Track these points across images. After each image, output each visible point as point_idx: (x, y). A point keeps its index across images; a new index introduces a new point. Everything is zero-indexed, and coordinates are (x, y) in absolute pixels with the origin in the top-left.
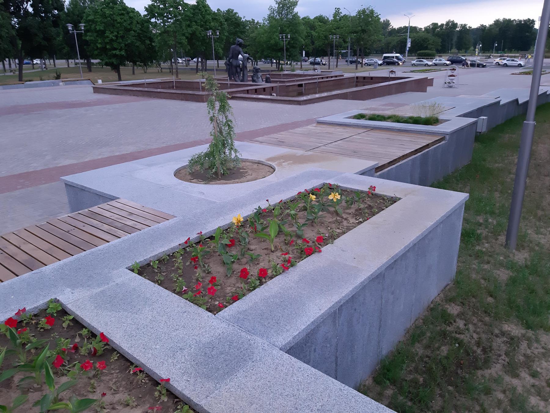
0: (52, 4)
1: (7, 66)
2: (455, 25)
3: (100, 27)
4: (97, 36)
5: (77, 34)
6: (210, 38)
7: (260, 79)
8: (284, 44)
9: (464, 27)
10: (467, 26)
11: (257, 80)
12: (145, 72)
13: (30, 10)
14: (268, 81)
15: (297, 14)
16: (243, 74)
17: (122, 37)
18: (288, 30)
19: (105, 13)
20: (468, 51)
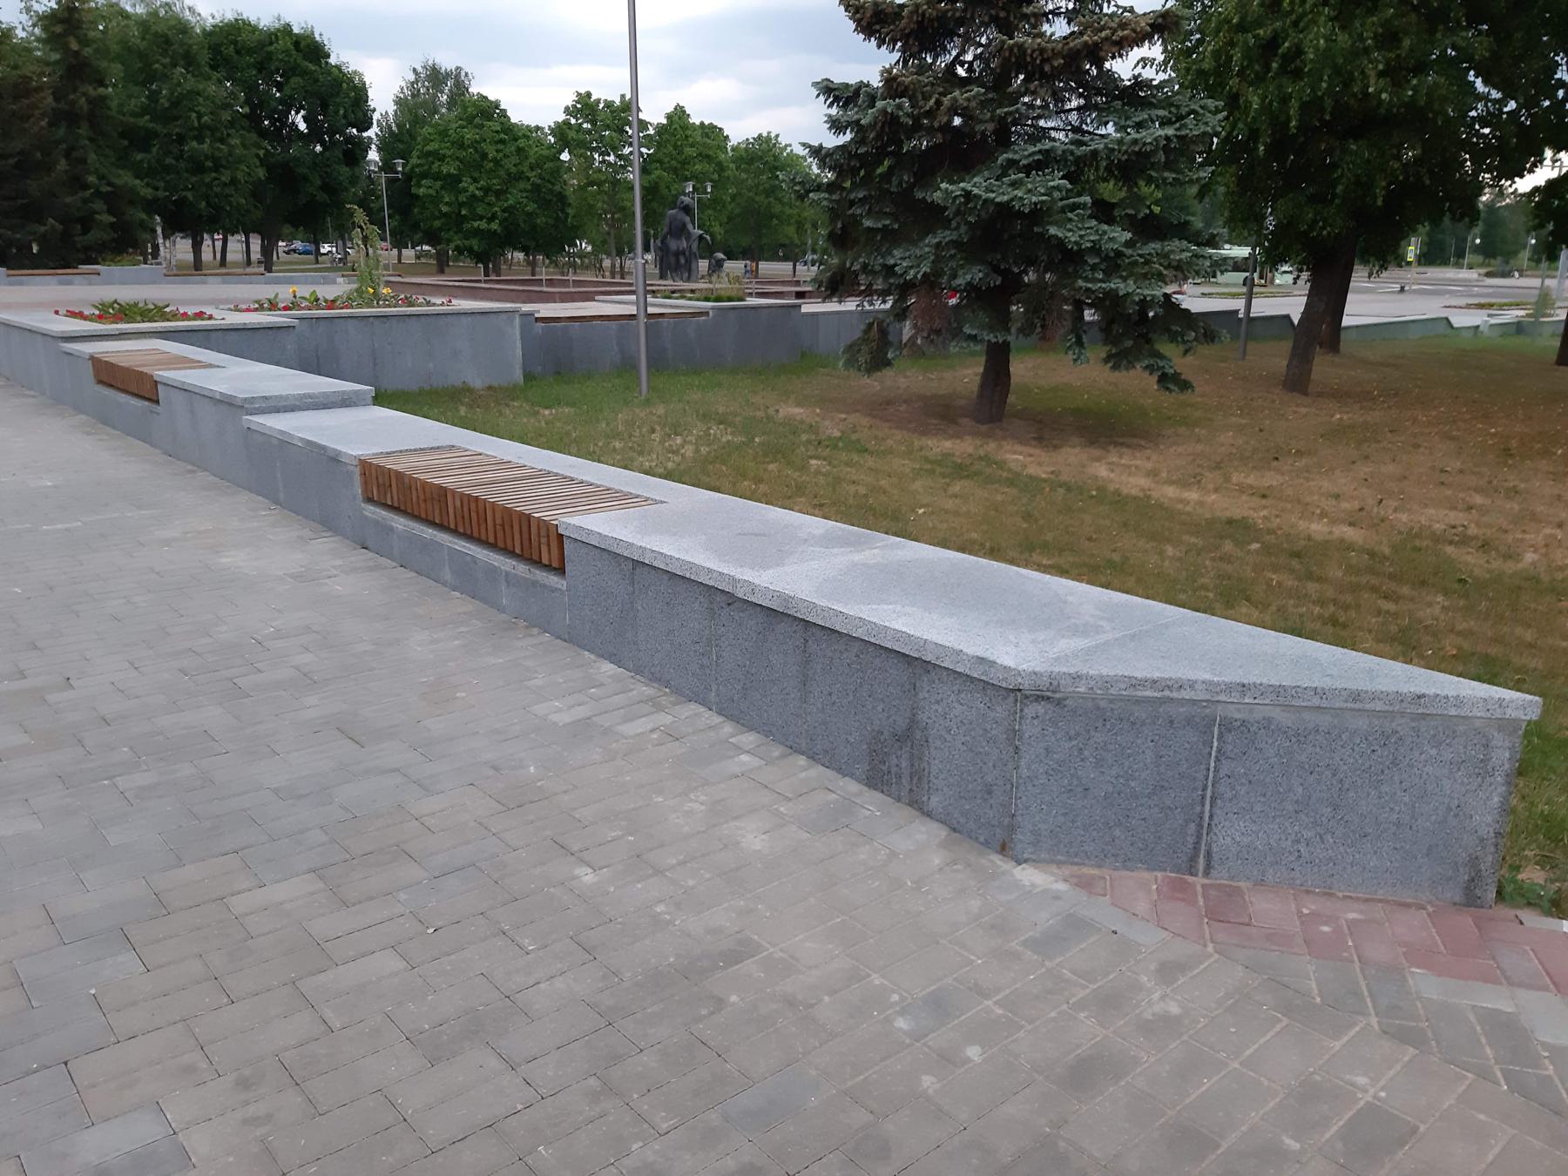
0: (345, 117)
1: (207, 254)
3: (449, 168)
4: (442, 188)
5: (388, 181)
10: (832, 141)
13: (302, 126)
17: (498, 194)
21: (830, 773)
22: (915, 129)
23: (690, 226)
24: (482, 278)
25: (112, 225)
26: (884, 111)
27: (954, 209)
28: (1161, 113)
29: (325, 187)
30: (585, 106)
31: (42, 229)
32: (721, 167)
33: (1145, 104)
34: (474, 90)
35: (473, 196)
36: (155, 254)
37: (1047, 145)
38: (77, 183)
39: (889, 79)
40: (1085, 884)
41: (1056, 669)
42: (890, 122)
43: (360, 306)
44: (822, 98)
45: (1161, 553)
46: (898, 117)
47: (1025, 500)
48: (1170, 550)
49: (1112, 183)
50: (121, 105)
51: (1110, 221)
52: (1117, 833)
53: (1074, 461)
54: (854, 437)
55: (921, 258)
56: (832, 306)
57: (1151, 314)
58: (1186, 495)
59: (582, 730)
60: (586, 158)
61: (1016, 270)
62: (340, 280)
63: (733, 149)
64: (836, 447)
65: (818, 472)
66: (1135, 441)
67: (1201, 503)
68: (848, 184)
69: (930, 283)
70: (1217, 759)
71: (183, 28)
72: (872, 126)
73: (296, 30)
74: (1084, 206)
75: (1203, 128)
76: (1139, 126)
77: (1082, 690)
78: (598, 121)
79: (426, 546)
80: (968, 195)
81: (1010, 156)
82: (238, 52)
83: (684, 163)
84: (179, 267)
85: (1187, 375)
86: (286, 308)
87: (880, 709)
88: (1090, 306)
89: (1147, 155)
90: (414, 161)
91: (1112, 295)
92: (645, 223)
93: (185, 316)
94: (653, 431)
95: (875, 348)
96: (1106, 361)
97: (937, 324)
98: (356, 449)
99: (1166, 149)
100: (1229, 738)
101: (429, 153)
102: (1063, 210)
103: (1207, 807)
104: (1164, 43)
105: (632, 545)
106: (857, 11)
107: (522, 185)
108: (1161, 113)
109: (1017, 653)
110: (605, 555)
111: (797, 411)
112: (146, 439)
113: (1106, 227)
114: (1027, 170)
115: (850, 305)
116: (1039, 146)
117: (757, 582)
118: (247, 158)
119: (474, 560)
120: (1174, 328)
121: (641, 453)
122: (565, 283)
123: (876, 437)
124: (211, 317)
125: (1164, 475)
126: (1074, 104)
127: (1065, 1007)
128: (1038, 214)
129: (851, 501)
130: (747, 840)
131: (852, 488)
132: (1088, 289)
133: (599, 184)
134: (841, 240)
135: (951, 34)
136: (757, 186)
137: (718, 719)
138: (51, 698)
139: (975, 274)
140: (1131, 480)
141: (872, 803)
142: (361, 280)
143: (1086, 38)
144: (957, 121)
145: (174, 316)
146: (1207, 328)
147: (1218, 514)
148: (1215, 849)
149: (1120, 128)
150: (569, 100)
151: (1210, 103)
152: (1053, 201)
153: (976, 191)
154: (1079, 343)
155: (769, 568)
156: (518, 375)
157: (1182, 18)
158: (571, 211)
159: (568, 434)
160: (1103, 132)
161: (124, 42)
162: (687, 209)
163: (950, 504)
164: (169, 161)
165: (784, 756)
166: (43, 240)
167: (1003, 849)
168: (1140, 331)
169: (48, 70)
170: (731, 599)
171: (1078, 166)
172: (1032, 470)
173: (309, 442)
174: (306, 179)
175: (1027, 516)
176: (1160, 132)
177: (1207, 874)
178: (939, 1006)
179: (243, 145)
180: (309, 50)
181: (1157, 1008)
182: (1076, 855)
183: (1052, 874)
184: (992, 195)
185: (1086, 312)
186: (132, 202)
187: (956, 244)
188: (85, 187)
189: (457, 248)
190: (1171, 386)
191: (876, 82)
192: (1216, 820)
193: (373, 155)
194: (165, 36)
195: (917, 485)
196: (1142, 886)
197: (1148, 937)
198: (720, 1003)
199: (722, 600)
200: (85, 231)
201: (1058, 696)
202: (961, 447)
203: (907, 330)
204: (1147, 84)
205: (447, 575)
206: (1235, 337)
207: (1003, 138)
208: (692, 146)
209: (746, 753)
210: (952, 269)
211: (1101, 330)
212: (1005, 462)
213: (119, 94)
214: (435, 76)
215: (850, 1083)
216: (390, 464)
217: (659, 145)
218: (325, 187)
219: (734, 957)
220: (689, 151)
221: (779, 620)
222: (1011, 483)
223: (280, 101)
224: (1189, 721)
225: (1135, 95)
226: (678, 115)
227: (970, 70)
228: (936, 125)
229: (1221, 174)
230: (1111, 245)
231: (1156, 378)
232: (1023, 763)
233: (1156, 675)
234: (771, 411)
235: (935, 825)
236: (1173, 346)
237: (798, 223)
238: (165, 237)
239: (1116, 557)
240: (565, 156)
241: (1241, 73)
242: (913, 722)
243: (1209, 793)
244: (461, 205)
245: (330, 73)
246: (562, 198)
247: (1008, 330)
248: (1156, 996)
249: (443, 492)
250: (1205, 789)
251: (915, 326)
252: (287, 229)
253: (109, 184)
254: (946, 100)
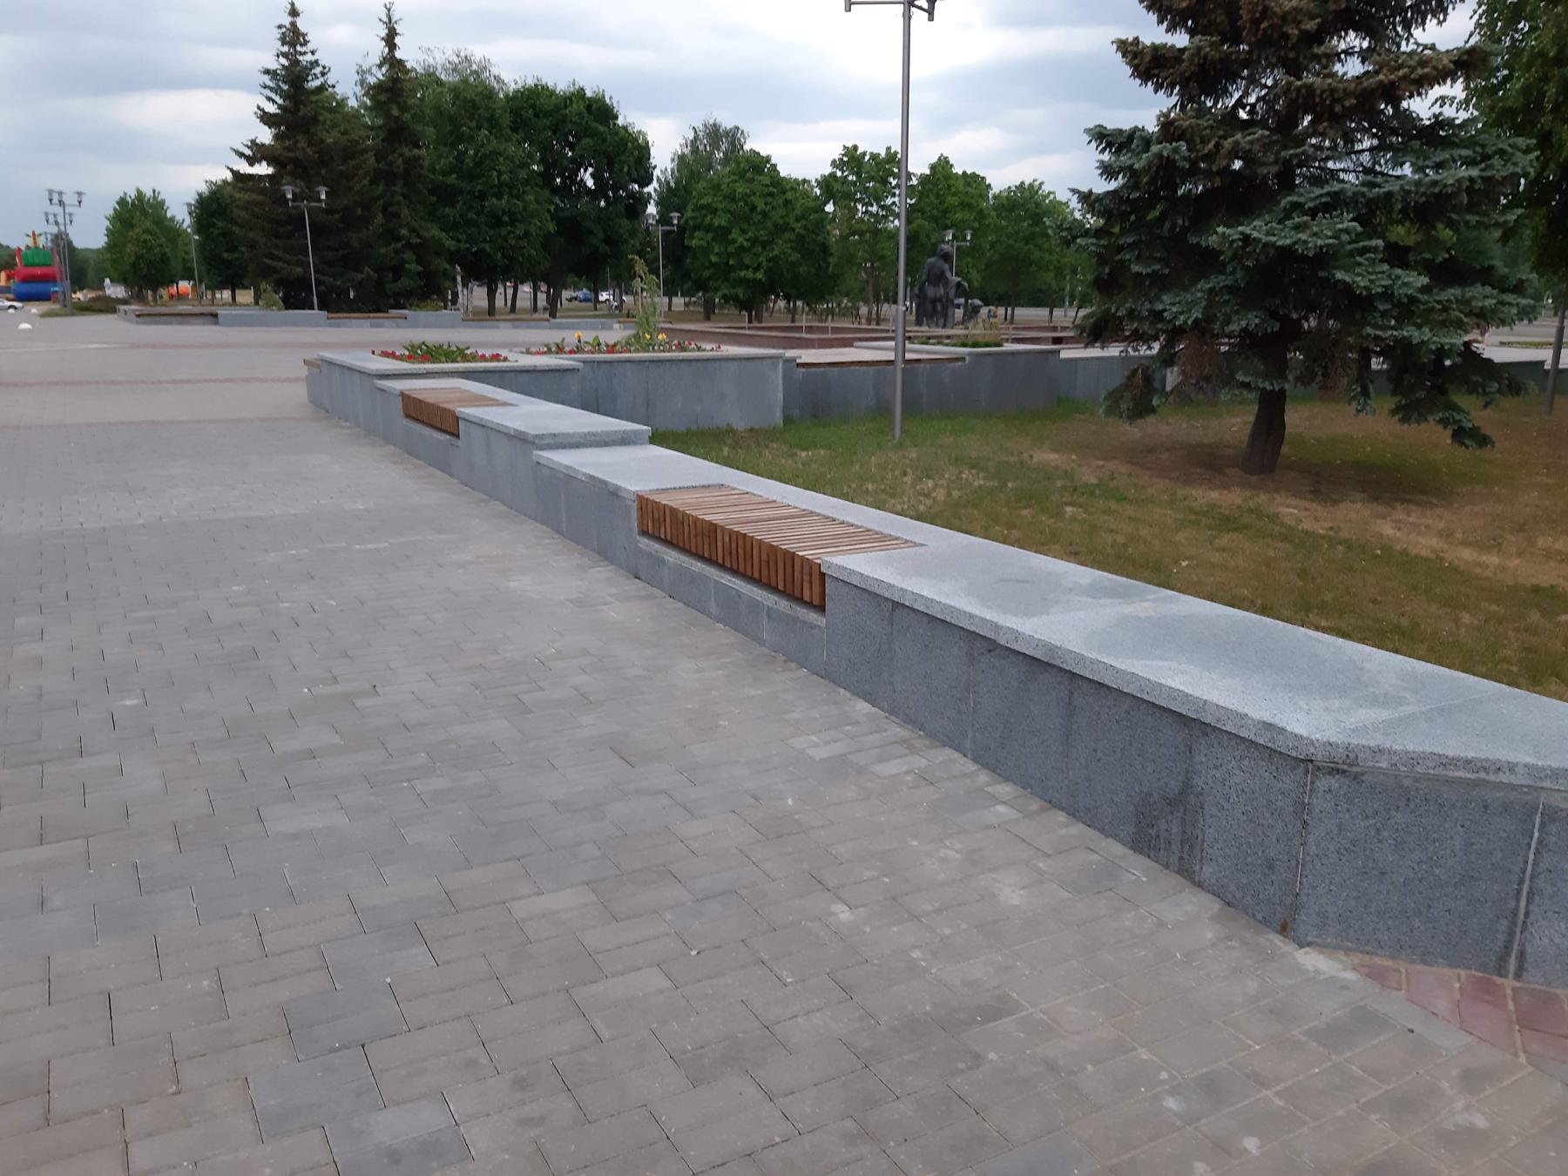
0: (629, 173)
1: (499, 302)
3: (721, 221)
10: (1102, 186)
13: (590, 183)
17: (764, 245)
21: (1091, 832)
22: (1192, 173)
23: (948, 274)
24: (746, 324)
25: (419, 273)
26: (1159, 156)
27: (1230, 254)
28: (1465, 152)
29: (608, 240)
30: (852, 159)
31: (359, 277)
32: (981, 215)
33: (1446, 143)
34: (747, 147)
35: (742, 247)
36: (455, 301)
37: (1336, 187)
38: (391, 235)
39: (1168, 127)
40: (1377, 975)
41: (1355, 741)
42: (1166, 171)
43: (637, 351)
44: (1094, 144)
45: (1457, 621)
46: (1174, 161)
47: (1299, 557)
48: (1466, 618)
49: (1407, 224)
50: (431, 165)
51: (1405, 265)
52: (1417, 923)
53: (1353, 517)
54: (1112, 484)
55: (1192, 304)
56: (1095, 352)
57: (1448, 363)
58: (1484, 558)
59: (838, 767)
60: (850, 209)
61: (1295, 316)
62: (616, 326)
63: (995, 197)
64: (1092, 494)
65: (1073, 519)
66: (1424, 498)
67: (1502, 568)
68: (1116, 230)
69: (1202, 329)
70: (1537, 852)
71: (488, 94)
72: (1146, 170)
73: (589, 94)
74: (1375, 250)
75: (1511, 169)
76: (1438, 166)
77: (1384, 765)
78: (864, 173)
79: (694, 579)
80: (1246, 239)
81: (1294, 198)
82: (536, 115)
83: (945, 212)
84: (474, 313)
85: (1486, 431)
86: (571, 352)
87: (1149, 770)
88: (1378, 354)
89: (1448, 197)
90: (689, 214)
91: (1405, 346)
92: (907, 273)
93: (483, 358)
94: (905, 474)
95: (1138, 394)
96: (1394, 412)
97: (1208, 370)
98: (634, 484)
99: (1469, 191)
100: (1553, 828)
101: (703, 207)
102: (1351, 254)
103: (1523, 903)
104: (1467, 80)
105: (893, 586)
106: (1135, 56)
107: (787, 235)
108: (1465, 152)
109: (1310, 720)
110: (865, 595)
111: (1052, 457)
112: (445, 468)
113: (1399, 271)
114: (1313, 213)
115: (1114, 351)
116: (1327, 189)
117: (1021, 629)
118: (539, 214)
119: (739, 594)
120: (1475, 378)
121: (893, 496)
122: (824, 330)
123: (1136, 486)
124: (505, 359)
125: (1459, 535)
126: (1367, 144)
127: (1354, 1106)
128: (1324, 258)
129: (1109, 550)
130: (999, 889)
131: (1110, 538)
132: (1377, 338)
133: (861, 234)
134: (1109, 283)
135: (1233, 77)
136: (1017, 233)
137: (973, 767)
138: (360, 703)
139: (1251, 320)
140: (1422, 540)
141: (1137, 868)
142: (639, 325)
143: (1381, 77)
144: (1237, 165)
145: (474, 358)
146: (1513, 378)
147: (1522, 581)
148: (1529, 950)
149: (1418, 169)
150: (836, 152)
151: (1521, 142)
152: (1342, 244)
153: (1255, 234)
154: (1365, 393)
155: (1033, 616)
156: (778, 417)
157: (1490, 54)
158: (832, 260)
159: (823, 475)
160: (1398, 172)
161: (438, 109)
162: (946, 257)
163: (1216, 557)
164: (471, 215)
165: (1043, 810)
166: (359, 287)
167: (1283, 929)
168: (1436, 382)
169: (372, 134)
170: (992, 646)
171: (1372, 208)
172: (1307, 525)
173: (592, 477)
174: (590, 232)
175: (1303, 574)
176: (1464, 172)
177: (1518, 976)
178: (1211, 1089)
179: (537, 201)
180: (599, 112)
181: (1461, 1119)
182: (1368, 942)
183: (1341, 962)
184: (1273, 239)
185: (1374, 360)
186: (437, 254)
187: (1231, 289)
188: (398, 239)
189: (724, 297)
190: (1468, 442)
191: (1152, 127)
192: (1532, 917)
193: (652, 209)
194: (473, 101)
195: (1180, 537)
196: (1444, 984)
197: (1450, 1040)
198: (978, 1058)
199: (983, 646)
200: (396, 278)
201: (1355, 769)
202: (1229, 498)
203: (1172, 378)
204: (1450, 123)
205: (713, 608)
206: (1543, 389)
207: (1286, 180)
208: (954, 194)
209: (1003, 805)
210: (1225, 314)
211: (1390, 380)
212: (1277, 515)
213: (429, 155)
214: (715, 134)
215: (1115, 1161)
216: (664, 500)
217: (921, 196)
218: (608, 240)
219: (996, 1010)
220: (950, 200)
221: (1043, 669)
222: (1285, 539)
223: (572, 160)
224: (1506, 808)
225: (1436, 135)
226: (942, 167)
227: (1252, 112)
228: (1215, 168)
229: (1527, 217)
230: (1404, 290)
231: (1449, 432)
232: (1311, 839)
233: (1471, 754)
234: (1025, 456)
235: (1208, 897)
236: (1473, 398)
237: (1056, 268)
238: (465, 285)
239: (1405, 622)
240: (829, 208)
241: (1556, 109)
242: (1187, 785)
243: (1526, 887)
244: (729, 255)
245: (617, 134)
246: (825, 248)
247: (1284, 377)
248: (1459, 1105)
249: (713, 528)
250: (1521, 882)
251: (1183, 373)
252: (571, 278)
253: (419, 236)
254: (1228, 143)
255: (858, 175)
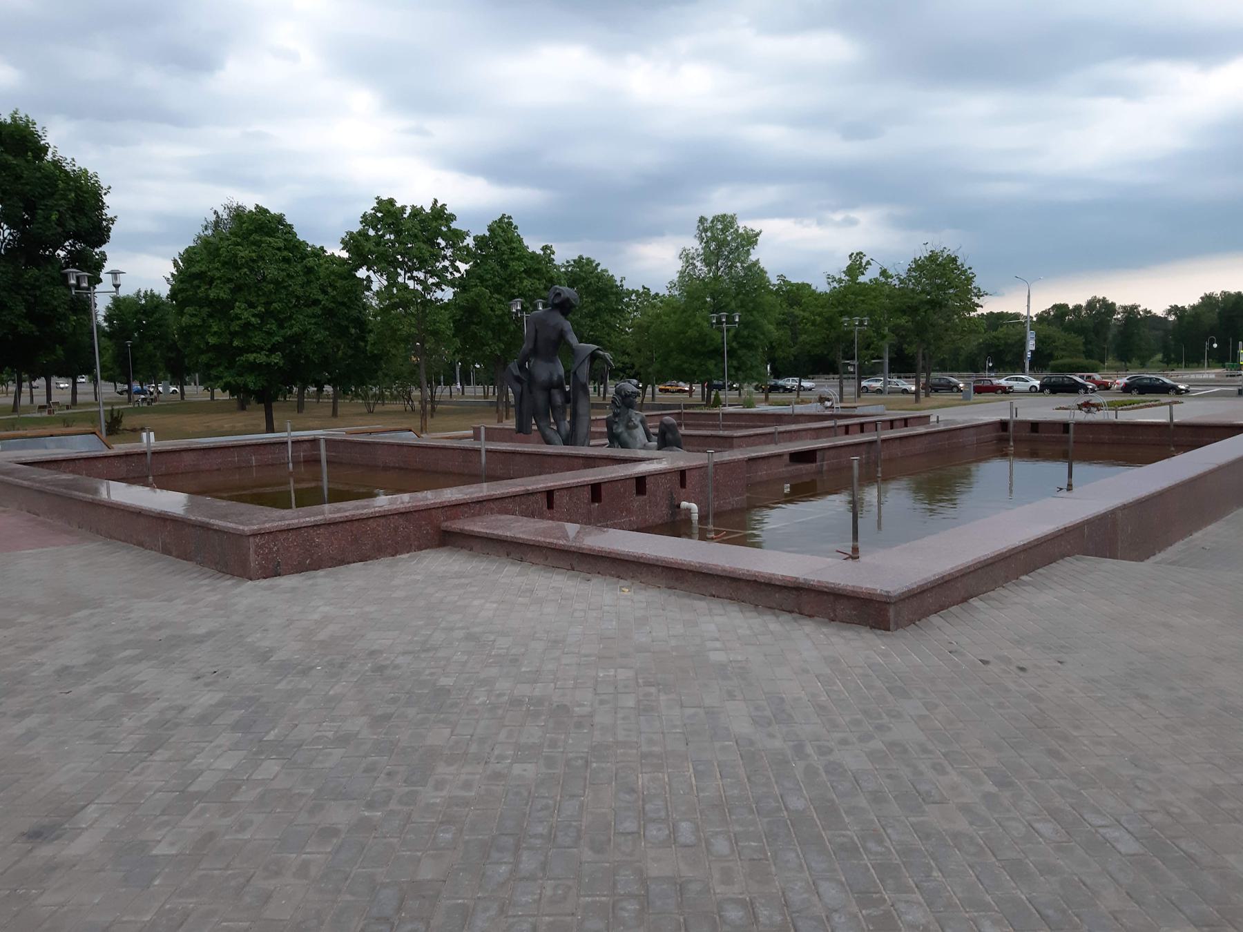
0: (60, 223)
1: (25, 400)
2: (1109, 308)
4: (210, 315)
6: (517, 318)
7: (640, 433)
8: (724, 339)
9: (1131, 311)
11: (630, 440)
12: (371, 412)
14: (667, 439)
15: (756, 263)
16: (574, 415)
18: (733, 304)
19: (236, 256)
20: (1148, 364)
23: (573, 339)
35: (248, 325)
150: (368, 207)
244: (234, 334)
246: (361, 324)
255: (398, 233)
